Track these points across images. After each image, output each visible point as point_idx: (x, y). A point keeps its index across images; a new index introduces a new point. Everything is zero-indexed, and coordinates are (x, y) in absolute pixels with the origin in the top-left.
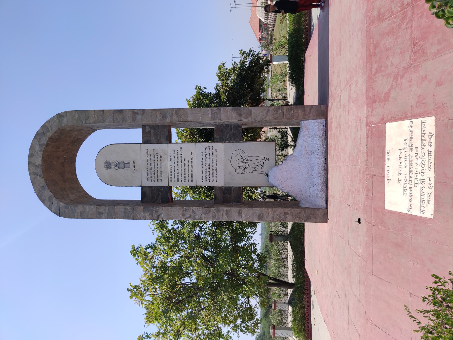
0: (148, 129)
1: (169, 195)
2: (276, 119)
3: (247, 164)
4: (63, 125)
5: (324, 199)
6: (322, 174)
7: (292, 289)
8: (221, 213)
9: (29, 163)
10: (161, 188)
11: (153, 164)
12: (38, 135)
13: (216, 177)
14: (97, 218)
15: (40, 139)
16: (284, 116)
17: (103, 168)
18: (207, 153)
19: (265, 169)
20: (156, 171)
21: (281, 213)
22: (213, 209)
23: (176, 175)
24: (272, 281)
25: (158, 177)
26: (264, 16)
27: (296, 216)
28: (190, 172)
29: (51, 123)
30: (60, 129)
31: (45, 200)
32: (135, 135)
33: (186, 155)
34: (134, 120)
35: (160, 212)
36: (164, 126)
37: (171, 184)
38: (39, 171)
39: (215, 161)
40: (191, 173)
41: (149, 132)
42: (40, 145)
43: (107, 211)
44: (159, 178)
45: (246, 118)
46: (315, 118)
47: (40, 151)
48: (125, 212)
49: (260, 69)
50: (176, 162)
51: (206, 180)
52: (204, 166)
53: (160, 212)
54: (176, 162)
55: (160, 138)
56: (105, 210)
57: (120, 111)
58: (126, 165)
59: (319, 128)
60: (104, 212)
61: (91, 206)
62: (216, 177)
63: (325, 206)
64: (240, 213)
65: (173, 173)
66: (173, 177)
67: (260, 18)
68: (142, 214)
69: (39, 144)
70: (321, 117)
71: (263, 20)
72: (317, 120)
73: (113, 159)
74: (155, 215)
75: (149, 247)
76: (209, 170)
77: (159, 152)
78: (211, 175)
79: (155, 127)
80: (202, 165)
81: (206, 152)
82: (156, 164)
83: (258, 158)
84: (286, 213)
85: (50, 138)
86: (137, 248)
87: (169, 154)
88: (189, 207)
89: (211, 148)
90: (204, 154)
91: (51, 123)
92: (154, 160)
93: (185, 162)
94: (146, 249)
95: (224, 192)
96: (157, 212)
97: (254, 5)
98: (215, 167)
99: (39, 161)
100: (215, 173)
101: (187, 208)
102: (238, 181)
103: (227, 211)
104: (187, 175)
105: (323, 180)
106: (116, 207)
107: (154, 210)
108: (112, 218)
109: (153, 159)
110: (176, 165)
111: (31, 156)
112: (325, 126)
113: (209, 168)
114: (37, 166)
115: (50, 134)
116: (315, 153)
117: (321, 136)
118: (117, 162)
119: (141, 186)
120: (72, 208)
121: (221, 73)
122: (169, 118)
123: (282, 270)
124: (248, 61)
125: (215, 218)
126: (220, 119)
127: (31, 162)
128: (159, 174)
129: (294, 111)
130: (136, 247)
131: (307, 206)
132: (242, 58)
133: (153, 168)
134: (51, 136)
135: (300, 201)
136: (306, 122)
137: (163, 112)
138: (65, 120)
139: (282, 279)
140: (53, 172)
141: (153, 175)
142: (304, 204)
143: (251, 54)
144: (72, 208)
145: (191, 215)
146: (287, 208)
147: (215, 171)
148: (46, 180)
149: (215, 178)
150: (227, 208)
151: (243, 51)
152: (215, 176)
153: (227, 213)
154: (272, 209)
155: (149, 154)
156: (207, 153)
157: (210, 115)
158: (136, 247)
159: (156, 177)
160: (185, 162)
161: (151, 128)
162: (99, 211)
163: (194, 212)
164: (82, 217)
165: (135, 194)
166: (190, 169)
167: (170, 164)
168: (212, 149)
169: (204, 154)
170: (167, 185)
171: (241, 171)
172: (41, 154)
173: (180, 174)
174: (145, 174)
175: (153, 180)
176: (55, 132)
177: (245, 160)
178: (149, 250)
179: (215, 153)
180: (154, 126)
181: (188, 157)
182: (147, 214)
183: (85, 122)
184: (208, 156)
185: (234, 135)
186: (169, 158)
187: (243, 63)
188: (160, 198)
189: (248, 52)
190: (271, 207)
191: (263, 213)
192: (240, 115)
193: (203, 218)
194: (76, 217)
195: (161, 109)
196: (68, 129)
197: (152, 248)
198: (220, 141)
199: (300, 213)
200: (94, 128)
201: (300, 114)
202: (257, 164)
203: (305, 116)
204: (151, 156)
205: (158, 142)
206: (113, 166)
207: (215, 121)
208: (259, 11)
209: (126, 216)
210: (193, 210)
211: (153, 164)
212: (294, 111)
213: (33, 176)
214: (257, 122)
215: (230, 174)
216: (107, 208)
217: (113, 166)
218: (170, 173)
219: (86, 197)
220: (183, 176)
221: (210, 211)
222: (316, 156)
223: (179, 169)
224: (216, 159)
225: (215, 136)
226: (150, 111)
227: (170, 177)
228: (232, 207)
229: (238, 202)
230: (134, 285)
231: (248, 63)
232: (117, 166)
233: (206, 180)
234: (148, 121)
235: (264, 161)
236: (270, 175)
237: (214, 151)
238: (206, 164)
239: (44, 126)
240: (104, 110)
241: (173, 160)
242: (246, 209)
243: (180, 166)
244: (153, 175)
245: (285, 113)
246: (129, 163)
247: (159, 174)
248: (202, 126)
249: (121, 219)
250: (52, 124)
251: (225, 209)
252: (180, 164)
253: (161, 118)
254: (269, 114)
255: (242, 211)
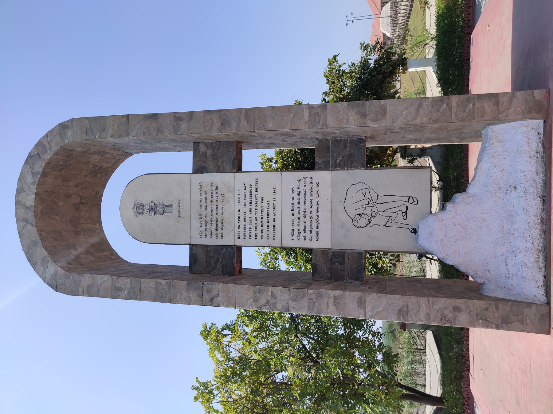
0: (202, 148)
1: (234, 261)
2: (435, 122)
3: (374, 209)
4: (66, 141)
5: (541, 283)
6: (537, 232)
7: (435, 407)
8: (325, 300)
9: (17, 203)
10: (222, 250)
11: (209, 208)
12: (31, 159)
13: (317, 232)
14: (113, 297)
15: (33, 165)
16: (454, 115)
17: (131, 212)
18: (302, 189)
19: (411, 220)
20: (214, 219)
21: (446, 308)
22: (310, 292)
23: (248, 227)
24: (405, 392)
25: (217, 229)
26: (390, 29)
27: (477, 315)
28: (272, 223)
29: (49, 139)
30: (62, 148)
31: (36, 263)
32: (184, 160)
33: (265, 192)
34: (176, 131)
35: (214, 293)
36: (228, 143)
37: (238, 243)
38: (31, 216)
39: (314, 204)
40: (273, 223)
41: (205, 154)
42: (34, 174)
43: (129, 285)
44: (220, 231)
45: (375, 120)
46: (521, 116)
47: (33, 183)
48: (157, 290)
49: (391, 68)
50: (248, 204)
51: (299, 236)
52: (296, 211)
53: (214, 293)
54: (248, 204)
55: (222, 163)
56: (125, 284)
57: (154, 117)
58: (167, 209)
59: (528, 139)
60: (123, 287)
61: (104, 276)
62: (317, 232)
63: (543, 299)
64: (361, 303)
65: (242, 223)
66: (241, 230)
67: (385, 32)
68: (185, 294)
69: (32, 173)
70: (533, 114)
71: (389, 35)
72: (525, 122)
73: (146, 199)
74: (207, 297)
75: (227, 327)
76: (305, 220)
77: (220, 186)
78: (308, 229)
79: (217, 146)
80: (293, 210)
81: (299, 188)
82: (214, 208)
83: (396, 198)
84: (457, 309)
85: (47, 164)
86: (210, 328)
87: (236, 190)
88: (266, 285)
89: (308, 180)
90: (296, 190)
91: (49, 139)
92: (211, 201)
93: (263, 205)
94: (223, 330)
95: (331, 259)
96: (209, 292)
97: (377, 16)
98: (314, 214)
99: (30, 200)
100: (315, 226)
101: (262, 288)
102: (357, 240)
103: (335, 298)
104: (265, 228)
105: (539, 243)
106: (142, 280)
107: (204, 287)
108: (136, 299)
109: (209, 199)
110: (247, 210)
111: (19, 191)
112: (541, 131)
113: (305, 217)
114: (27, 208)
115: (47, 156)
116: (519, 189)
117: (533, 153)
118: (153, 204)
119: (190, 245)
120: (76, 277)
121: (331, 71)
122: (234, 125)
123: (418, 367)
124: (373, 59)
125: (313, 309)
126: (325, 125)
127: (19, 202)
128: (220, 225)
129: (474, 105)
130: (208, 327)
131: (500, 294)
132: (364, 54)
133: (209, 215)
134: (50, 160)
135: (483, 284)
136: (498, 128)
137: (223, 116)
138: (69, 133)
139: (419, 389)
140: (57, 218)
141: (209, 226)
142: (491, 290)
143: (379, 46)
144: (76, 277)
145: (268, 302)
146: (459, 298)
147: (314, 221)
148: (40, 231)
149: (314, 234)
150: (337, 293)
151: (366, 44)
152: (314, 230)
153: (337, 302)
154: (425, 299)
155: (204, 189)
156: (302, 189)
157: (306, 117)
158: (208, 327)
159: (214, 230)
160: (263, 205)
161: (208, 147)
162: (116, 285)
163: (273, 296)
164: (90, 294)
165: (180, 257)
166: (271, 217)
167: (238, 207)
168: (311, 183)
169: (296, 190)
170: (231, 243)
171: (363, 222)
172: (34, 189)
173: (253, 225)
174: (196, 223)
175: (208, 235)
176: (56, 154)
177: (371, 202)
178: (226, 332)
179: (315, 189)
180: (212, 143)
181: (268, 196)
182: (193, 295)
183: (100, 136)
184: (302, 195)
185: (351, 156)
186: (237, 196)
187: (365, 63)
188: (219, 265)
189: (374, 43)
190: (424, 295)
191: (407, 306)
192: (364, 116)
193: (290, 308)
194: (80, 293)
195: (220, 111)
196: (80, 149)
197: (230, 329)
198: (326, 167)
199: (487, 309)
200: (128, 151)
201: (488, 110)
202: (395, 210)
203: (499, 113)
204: (206, 193)
205: (220, 170)
206: (148, 211)
207: (315, 129)
208: (383, 23)
209: (159, 297)
210: (272, 292)
211: (209, 208)
212: (474, 105)
213: (22, 224)
214: (397, 129)
215: (342, 227)
216: (128, 280)
217: (146, 211)
218: (237, 224)
219: (111, 259)
220: (259, 228)
221: (303, 296)
222: (522, 194)
223: (253, 216)
224: (318, 199)
225: (317, 160)
226: (202, 114)
227: (237, 230)
228: (345, 289)
229: (356, 279)
230: (203, 380)
231: (372, 62)
232: (153, 209)
233: (299, 236)
234: (200, 134)
235: (408, 204)
236: (420, 231)
237: (314, 185)
238: (299, 208)
239: (40, 144)
240: (128, 115)
241: (242, 201)
242: (374, 295)
243: (253, 211)
244: (209, 226)
245: (454, 109)
246: (171, 205)
247: (220, 225)
248: (294, 144)
249: (150, 301)
250: (51, 141)
251: (333, 293)
252: (253, 207)
253: (220, 125)
254: (421, 112)
255: (365, 300)
